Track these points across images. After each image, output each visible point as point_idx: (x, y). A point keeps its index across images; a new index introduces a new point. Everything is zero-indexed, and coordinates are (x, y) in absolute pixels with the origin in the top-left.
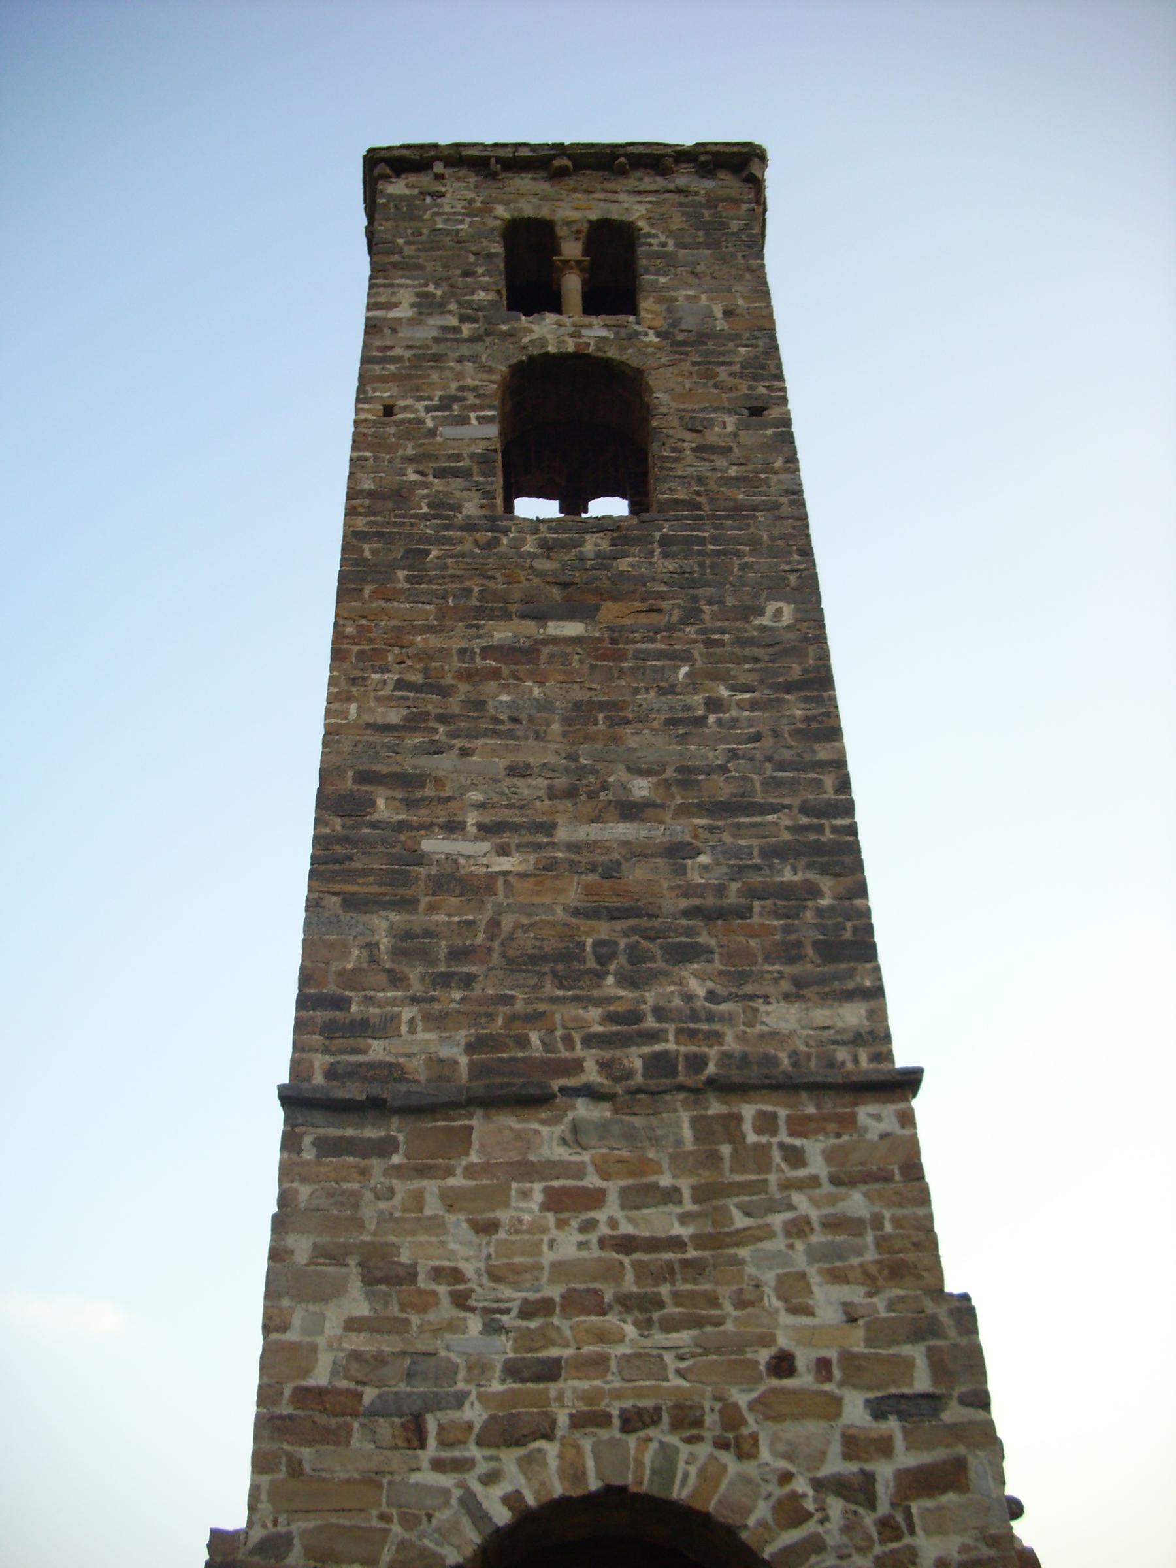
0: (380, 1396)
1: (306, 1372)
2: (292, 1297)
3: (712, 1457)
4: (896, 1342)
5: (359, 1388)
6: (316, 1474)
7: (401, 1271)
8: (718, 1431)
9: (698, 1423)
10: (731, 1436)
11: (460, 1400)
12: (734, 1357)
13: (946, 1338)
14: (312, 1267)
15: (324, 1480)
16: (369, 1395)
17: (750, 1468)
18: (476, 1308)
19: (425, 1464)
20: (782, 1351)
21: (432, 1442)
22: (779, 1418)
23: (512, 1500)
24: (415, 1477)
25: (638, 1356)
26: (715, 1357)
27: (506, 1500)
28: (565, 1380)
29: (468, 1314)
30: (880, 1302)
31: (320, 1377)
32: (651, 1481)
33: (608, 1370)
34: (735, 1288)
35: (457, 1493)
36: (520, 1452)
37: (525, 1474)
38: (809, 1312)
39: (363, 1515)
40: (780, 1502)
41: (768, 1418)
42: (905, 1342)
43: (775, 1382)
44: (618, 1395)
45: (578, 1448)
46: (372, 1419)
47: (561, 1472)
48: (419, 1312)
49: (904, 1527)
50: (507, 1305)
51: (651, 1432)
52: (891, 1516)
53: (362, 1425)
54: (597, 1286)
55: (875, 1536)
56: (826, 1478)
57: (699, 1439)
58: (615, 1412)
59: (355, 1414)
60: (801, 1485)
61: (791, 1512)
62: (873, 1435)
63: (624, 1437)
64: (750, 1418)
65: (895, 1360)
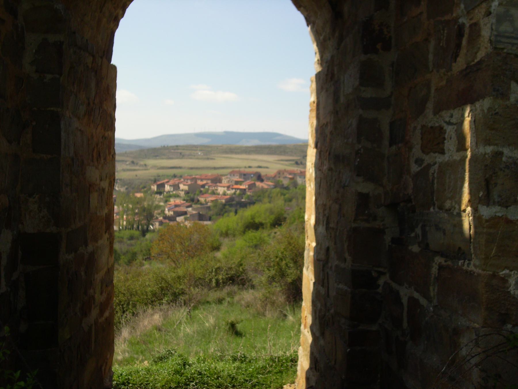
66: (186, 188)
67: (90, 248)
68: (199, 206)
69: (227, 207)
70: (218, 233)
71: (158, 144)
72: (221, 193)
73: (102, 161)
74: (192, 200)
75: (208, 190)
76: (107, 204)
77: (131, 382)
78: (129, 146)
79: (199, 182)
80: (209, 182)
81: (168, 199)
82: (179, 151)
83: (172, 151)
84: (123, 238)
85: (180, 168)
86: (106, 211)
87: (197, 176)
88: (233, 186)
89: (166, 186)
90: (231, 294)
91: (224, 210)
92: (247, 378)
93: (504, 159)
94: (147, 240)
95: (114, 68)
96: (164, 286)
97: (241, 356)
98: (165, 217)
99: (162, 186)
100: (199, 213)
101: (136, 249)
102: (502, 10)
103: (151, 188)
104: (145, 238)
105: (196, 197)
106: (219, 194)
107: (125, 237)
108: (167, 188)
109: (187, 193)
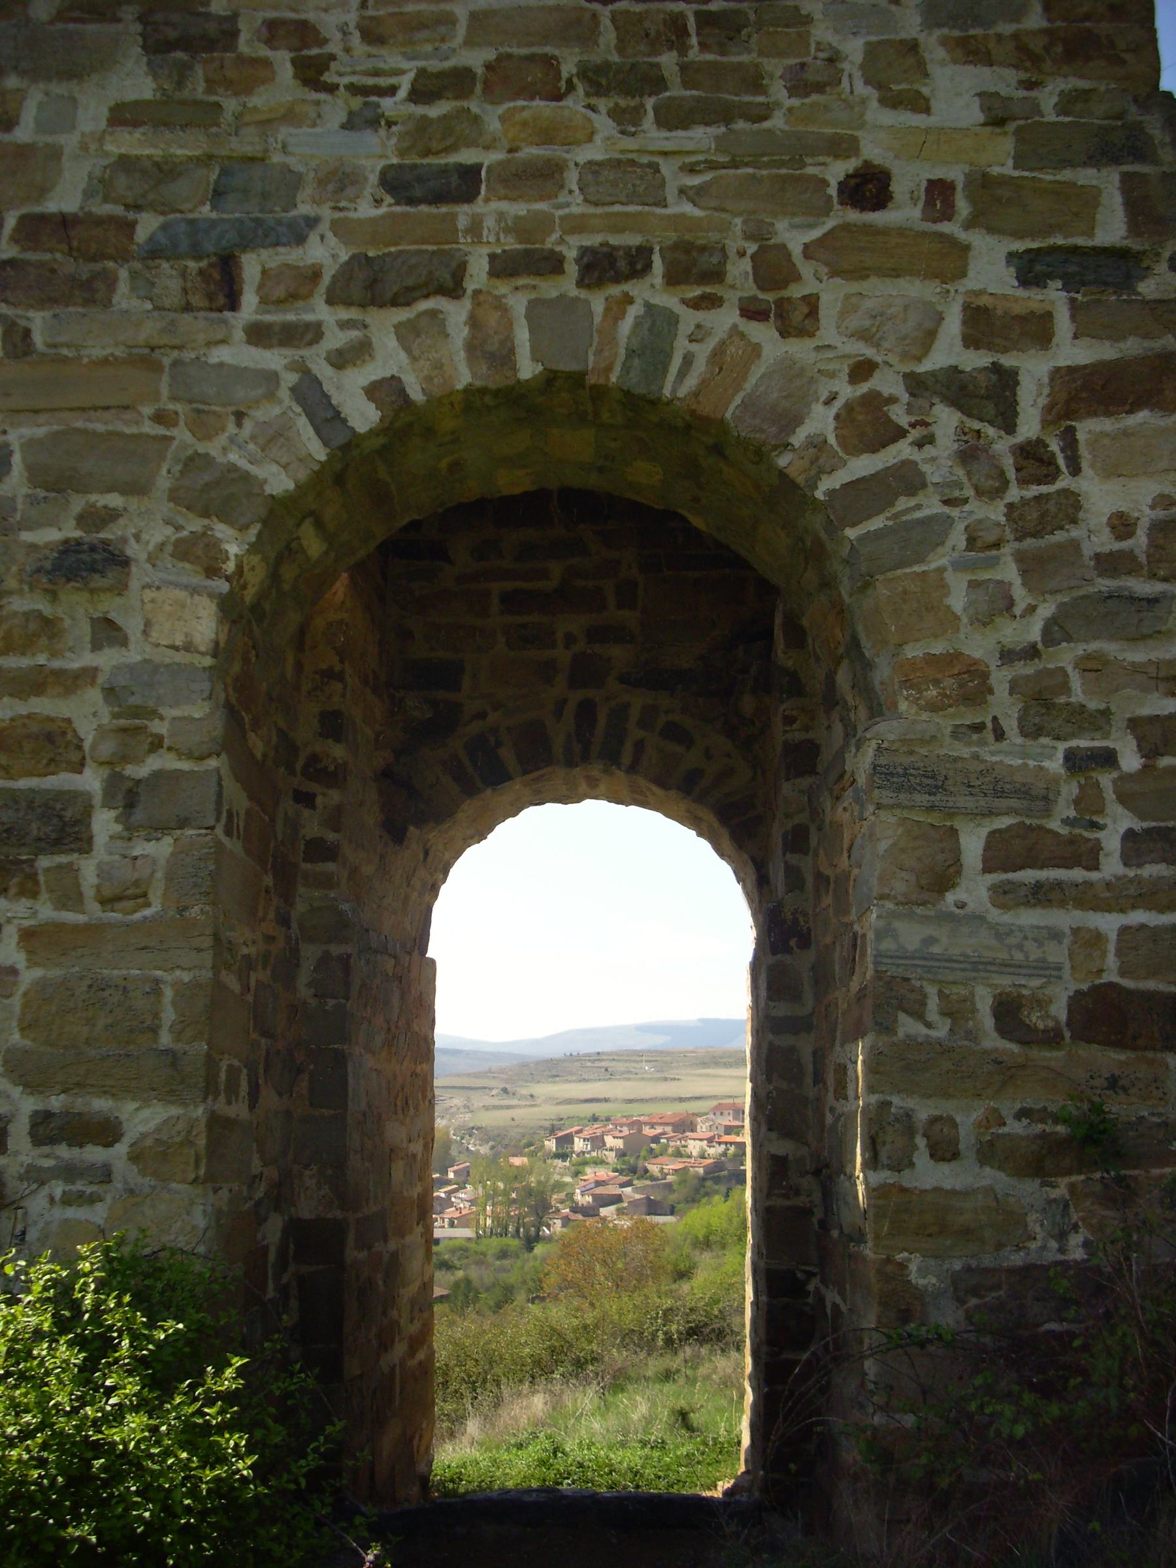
0: (164, 227)
1: (43, 192)
2: (23, 74)
3: (734, 330)
4: (1070, 164)
5: (131, 216)
6: (52, 351)
7: (212, 28)
8: (750, 289)
9: (716, 275)
10: (770, 297)
11: (298, 234)
12: (783, 171)
13: (1156, 162)
14: (60, 26)
15: (65, 360)
16: (147, 225)
17: (800, 349)
18: (337, 86)
19: (239, 335)
20: (867, 164)
21: (250, 299)
22: (859, 273)
23: (386, 391)
24: (220, 354)
25: (615, 164)
26: (750, 170)
27: (372, 391)
28: (487, 200)
29: (322, 96)
30: (1048, 98)
31: (66, 199)
32: (626, 368)
33: (562, 187)
34: (792, 61)
35: (290, 378)
36: (402, 315)
37: (408, 350)
38: (921, 105)
39: (128, 415)
40: (849, 407)
41: (834, 273)
42: (1084, 165)
43: (853, 216)
44: (577, 225)
45: (500, 306)
46: (150, 263)
47: (471, 348)
48: (236, 94)
49: (1061, 462)
50: (392, 81)
51: (633, 288)
52: (1040, 443)
53: (134, 275)
54: (548, 50)
55: (1011, 474)
56: (933, 374)
57: (711, 302)
58: (571, 254)
59: (123, 256)
60: (888, 383)
61: (868, 425)
62: (1018, 309)
63: (583, 294)
64: (806, 269)
65: (1063, 192)
66: (619, 1144)
67: (392, 1245)
68: (648, 1182)
69: (709, 1183)
70: (688, 1241)
71: (557, 1051)
72: (695, 1153)
73: (412, 1111)
74: (633, 1170)
75: (667, 1146)
76: (420, 1179)
77: (465, 1478)
78: (497, 1056)
79: (648, 1131)
80: (669, 1129)
81: (580, 1168)
82: (603, 1064)
83: (589, 1064)
84: (484, 1254)
85: (606, 1100)
86: (418, 1189)
87: (642, 1119)
88: (719, 1136)
89: (576, 1139)
90: (694, 1362)
91: (702, 1191)
92: (660, 1473)
93: (893, 1110)
94: (535, 1258)
95: (433, 962)
96: (557, 1344)
97: (655, 1441)
98: (575, 1209)
99: (568, 1140)
100: (648, 1198)
101: (512, 1278)
102: (881, 923)
103: (543, 1146)
104: (531, 1255)
105: (640, 1163)
106: (690, 1157)
107: (490, 1253)
108: (579, 1145)
109: (621, 1154)
